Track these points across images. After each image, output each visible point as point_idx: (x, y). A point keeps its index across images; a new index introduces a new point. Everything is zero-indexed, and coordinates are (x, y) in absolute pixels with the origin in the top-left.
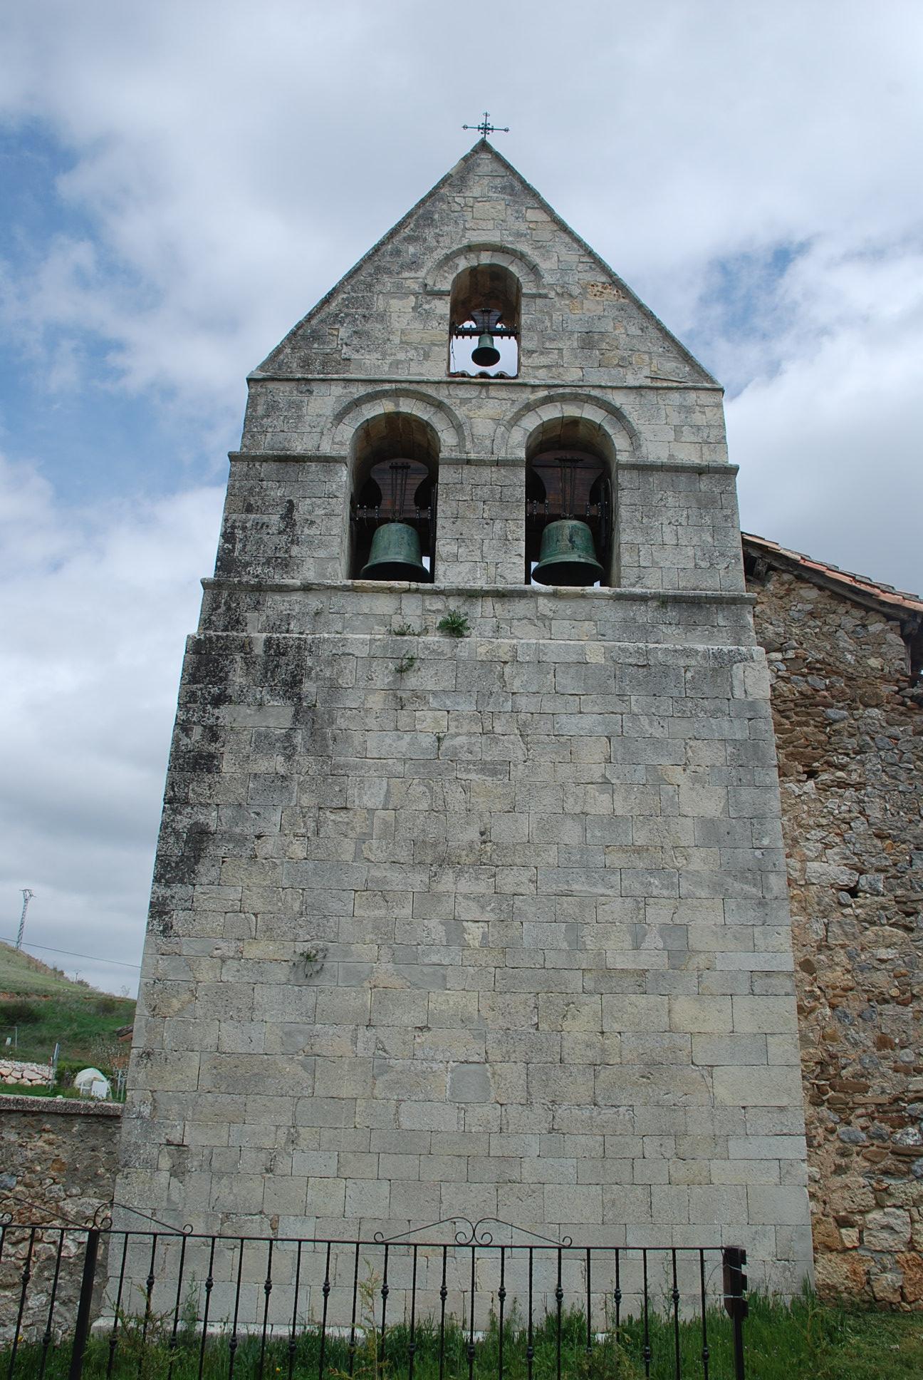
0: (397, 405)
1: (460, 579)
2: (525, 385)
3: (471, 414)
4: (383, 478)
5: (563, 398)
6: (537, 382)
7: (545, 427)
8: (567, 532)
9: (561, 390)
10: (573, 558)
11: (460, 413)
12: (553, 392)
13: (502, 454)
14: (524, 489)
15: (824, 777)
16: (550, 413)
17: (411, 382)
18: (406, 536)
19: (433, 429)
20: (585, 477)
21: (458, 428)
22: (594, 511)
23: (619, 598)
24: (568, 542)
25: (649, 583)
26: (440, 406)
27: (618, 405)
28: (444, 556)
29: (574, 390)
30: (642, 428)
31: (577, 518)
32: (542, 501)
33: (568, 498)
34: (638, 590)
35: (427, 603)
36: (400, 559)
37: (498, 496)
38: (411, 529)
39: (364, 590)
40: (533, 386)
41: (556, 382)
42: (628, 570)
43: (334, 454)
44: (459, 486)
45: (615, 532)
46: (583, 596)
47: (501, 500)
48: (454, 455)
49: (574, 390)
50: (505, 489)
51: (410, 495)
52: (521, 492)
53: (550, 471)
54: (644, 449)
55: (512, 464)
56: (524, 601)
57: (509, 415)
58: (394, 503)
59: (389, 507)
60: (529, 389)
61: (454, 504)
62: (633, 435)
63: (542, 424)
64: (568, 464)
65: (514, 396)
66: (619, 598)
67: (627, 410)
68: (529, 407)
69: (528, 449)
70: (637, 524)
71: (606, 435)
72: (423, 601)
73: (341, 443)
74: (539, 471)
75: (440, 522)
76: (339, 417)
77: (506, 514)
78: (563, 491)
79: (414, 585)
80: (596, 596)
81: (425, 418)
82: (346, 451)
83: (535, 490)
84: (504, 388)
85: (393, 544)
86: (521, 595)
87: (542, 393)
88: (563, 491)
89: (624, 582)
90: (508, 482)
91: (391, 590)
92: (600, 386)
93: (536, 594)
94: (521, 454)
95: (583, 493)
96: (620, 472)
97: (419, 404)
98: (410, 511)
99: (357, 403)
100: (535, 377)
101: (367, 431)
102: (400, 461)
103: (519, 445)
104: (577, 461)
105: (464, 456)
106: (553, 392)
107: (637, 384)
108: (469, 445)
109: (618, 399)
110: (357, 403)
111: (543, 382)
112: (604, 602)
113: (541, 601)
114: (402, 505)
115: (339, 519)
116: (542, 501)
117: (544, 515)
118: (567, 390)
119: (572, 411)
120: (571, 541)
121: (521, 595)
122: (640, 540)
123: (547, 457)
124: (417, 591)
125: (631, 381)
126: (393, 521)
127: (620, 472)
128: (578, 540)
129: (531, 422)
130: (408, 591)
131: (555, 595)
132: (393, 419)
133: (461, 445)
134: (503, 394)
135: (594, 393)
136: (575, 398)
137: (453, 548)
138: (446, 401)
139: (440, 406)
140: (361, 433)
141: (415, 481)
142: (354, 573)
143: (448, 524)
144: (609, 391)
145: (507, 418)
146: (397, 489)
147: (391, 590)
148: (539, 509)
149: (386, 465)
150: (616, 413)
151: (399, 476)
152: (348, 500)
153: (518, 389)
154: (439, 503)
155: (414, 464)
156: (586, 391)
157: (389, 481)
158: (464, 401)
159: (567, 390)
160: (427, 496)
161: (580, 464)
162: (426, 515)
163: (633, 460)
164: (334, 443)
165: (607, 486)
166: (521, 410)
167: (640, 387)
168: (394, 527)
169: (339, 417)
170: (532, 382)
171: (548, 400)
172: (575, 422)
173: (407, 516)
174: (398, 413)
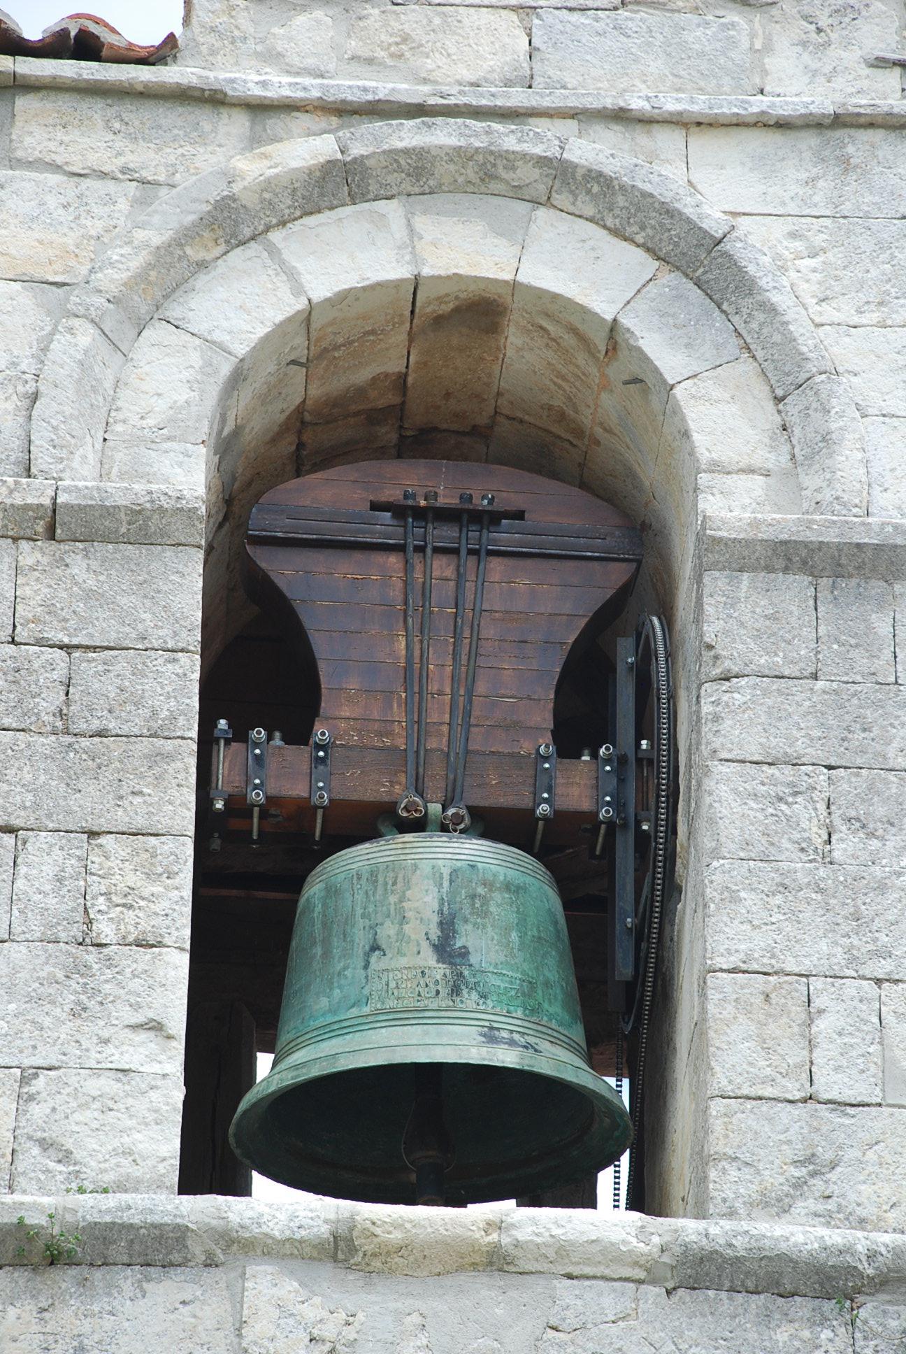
2: (213, 99)
5: (418, 177)
6: (280, 86)
7: (318, 336)
8: (424, 902)
9: (408, 135)
10: (456, 1042)
12: (366, 140)
13: (78, 477)
14: (192, 666)
16: (352, 257)
17: (417, 763)
20: (533, 607)
22: (578, 787)
23: (699, 1273)
24: (430, 958)
25: (863, 1193)
27: (712, 217)
29: (475, 134)
30: (844, 350)
31: (492, 824)
32: (298, 734)
33: (438, 713)
34: (800, 1234)
37: (51, 700)
40: (260, 109)
41: (384, 87)
42: (748, 1118)
45: (686, 908)
46: (497, 1261)
47: (64, 725)
49: (475, 134)
50: (88, 666)
52: (177, 687)
53: (345, 568)
54: (848, 461)
55: (137, 528)
56: (166, 1290)
57: (123, 264)
60: (236, 124)
62: (789, 383)
63: (307, 318)
64: (445, 534)
65: (148, 158)
66: (699, 1273)
67: (762, 246)
68: (232, 225)
69: (225, 447)
70: (800, 868)
71: (645, 383)
74: (285, 570)
77: (90, 802)
78: (413, 676)
80: (573, 1266)
83: (257, 667)
84: (97, 110)
85: (430, 958)
86: (156, 1251)
87: (306, 148)
88: (413, 676)
89: (726, 1183)
90: (103, 629)
92: (620, 116)
93: (237, 1247)
94: (188, 478)
95: (521, 696)
96: (716, 582)
100: (272, 57)
103: (169, 431)
104: (491, 518)
106: (366, 140)
107: (822, 101)
109: (715, 187)
111: (313, 88)
112: (609, 1300)
113: (267, 1287)
116: (298, 734)
117: (304, 809)
118: (444, 135)
119: (462, 248)
120: (446, 949)
121: (156, 1251)
122: (817, 950)
123: (333, 494)
125: (796, 88)
127: (716, 582)
128: (486, 946)
129: (246, 307)
131: (340, 1251)
134: (91, 139)
135: (590, 149)
136: (486, 179)
144: (668, 140)
145: (112, 279)
148: (278, 773)
150: (699, 261)
153: (171, 117)
156: (542, 140)
159: (444, 135)
161: (504, 537)
163: (784, 521)
165: (646, 655)
166: (187, 236)
167: (839, 122)
170: (251, 79)
171: (340, 185)
172: (479, 312)
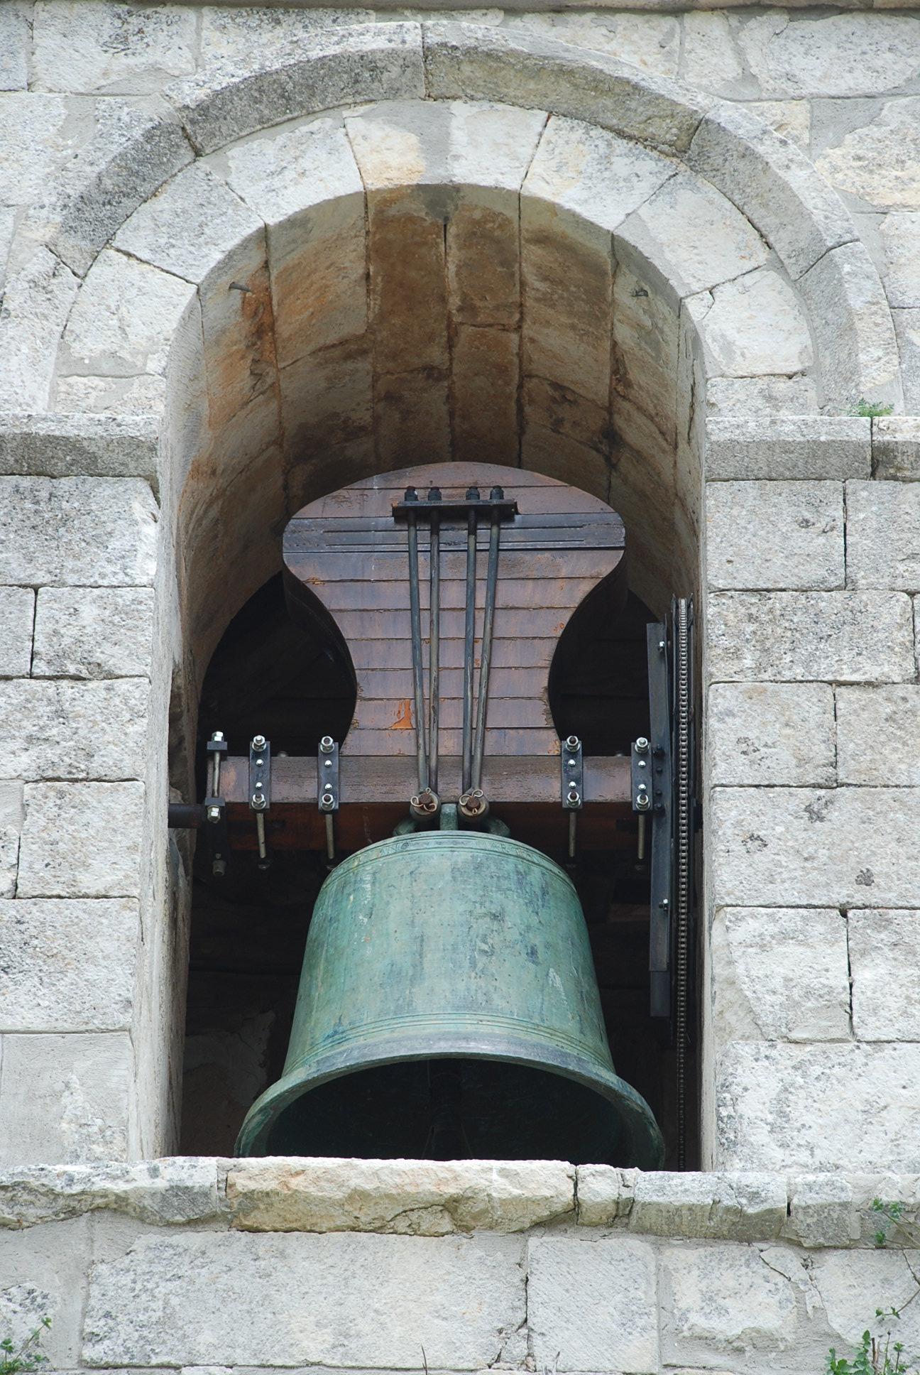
0: (437, 146)
1: (875, 1148)
3: (884, 189)
4: (351, 561)
11: (817, 180)
15: (262, 1263)
18: (516, 911)
19: (651, 283)
21: (808, 268)
26: (688, 144)
28: (769, 1006)
35: (688, 1293)
36: (488, 1038)
38: (539, 868)
39: (300, 1219)
43: (77, 425)
44: (831, 603)
48: (796, 423)
51: (524, 675)
58: (425, 717)
59: (402, 744)
61: (811, 704)
72: (664, 1277)
73: (118, 370)
75: (726, 814)
76: (100, 214)
79: (601, 1182)
81: (607, 214)
82: (148, 406)
85: (438, 949)
91: (460, 1215)
97: (569, 139)
98: (527, 765)
99: (197, 133)
101: (258, 300)
102: (452, 480)
105: (857, 430)
108: (876, 370)
110: (197, 133)
114: (475, 729)
115: (124, 800)
124: (622, 1216)
126: (431, 822)
130: (567, 1218)
132: (408, 233)
133: (827, 366)
137: (817, 960)
138: (726, 114)
139: (688, 144)
140: (225, 310)
141: (547, 593)
142: (203, 1112)
143: (780, 818)
146: (448, 639)
147: (460, 1215)
149: (373, 501)
151: (453, 567)
152: (164, 699)
154: (717, 700)
155: (537, 496)
157: (398, 596)
158: (838, 113)
160: (625, 666)
162: (618, 782)
164: (70, 366)
168: (440, 854)
169: (100, 214)
173: (512, 792)
174: (441, 198)
